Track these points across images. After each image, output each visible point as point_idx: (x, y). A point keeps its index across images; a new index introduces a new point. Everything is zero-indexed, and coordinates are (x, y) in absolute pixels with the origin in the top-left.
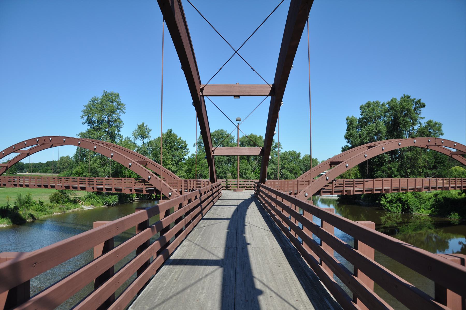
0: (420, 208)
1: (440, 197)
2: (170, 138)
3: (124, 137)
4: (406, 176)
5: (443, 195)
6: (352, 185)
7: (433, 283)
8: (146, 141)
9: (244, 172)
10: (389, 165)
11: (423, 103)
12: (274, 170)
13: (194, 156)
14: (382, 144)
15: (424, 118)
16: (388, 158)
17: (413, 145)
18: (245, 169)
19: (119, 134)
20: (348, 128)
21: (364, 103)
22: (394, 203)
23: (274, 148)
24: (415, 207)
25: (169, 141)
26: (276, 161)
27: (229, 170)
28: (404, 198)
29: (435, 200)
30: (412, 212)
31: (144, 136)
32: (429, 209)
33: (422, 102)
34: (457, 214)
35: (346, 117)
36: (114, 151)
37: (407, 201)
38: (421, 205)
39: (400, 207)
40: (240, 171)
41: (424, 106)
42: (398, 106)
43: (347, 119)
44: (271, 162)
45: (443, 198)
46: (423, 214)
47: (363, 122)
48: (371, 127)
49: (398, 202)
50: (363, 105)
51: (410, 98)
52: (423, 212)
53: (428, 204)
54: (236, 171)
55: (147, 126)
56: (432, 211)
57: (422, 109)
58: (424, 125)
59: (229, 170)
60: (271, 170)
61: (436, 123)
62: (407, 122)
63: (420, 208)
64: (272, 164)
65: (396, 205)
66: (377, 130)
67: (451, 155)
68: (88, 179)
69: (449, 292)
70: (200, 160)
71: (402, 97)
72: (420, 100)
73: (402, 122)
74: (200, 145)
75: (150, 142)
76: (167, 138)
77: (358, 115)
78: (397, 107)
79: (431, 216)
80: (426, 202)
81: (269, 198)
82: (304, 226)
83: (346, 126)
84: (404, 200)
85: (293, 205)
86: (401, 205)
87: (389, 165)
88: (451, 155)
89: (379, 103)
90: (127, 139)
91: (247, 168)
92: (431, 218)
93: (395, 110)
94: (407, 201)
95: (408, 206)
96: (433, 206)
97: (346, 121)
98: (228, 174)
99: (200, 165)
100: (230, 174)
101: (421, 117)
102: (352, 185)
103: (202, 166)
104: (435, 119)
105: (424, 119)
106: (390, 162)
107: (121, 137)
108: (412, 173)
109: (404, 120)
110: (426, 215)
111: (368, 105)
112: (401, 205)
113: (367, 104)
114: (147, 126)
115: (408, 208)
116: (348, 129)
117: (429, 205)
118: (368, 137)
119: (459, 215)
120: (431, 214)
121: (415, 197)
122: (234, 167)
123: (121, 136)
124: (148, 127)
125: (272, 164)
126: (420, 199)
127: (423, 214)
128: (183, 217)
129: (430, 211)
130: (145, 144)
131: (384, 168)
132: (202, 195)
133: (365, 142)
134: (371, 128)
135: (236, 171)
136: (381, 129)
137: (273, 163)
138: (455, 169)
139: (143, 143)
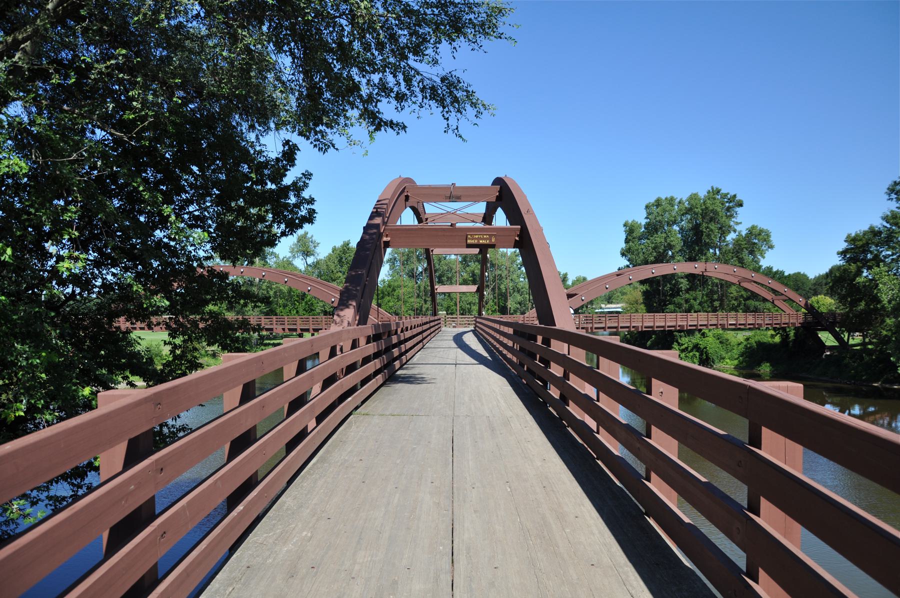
0: (724, 358)
1: (752, 341)
2: (348, 255)
3: (281, 257)
4: (715, 310)
5: (757, 338)
6: (591, 321)
7: (563, 369)
8: (310, 260)
9: (468, 309)
10: (687, 296)
11: (740, 200)
12: (520, 303)
13: (384, 283)
14: (630, 273)
15: (741, 223)
16: (684, 284)
17: (674, 272)
18: (470, 304)
19: (272, 252)
20: (626, 239)
21: (652, 200)
22: (689, 352)
23: (519, 266)
24: (717, 357)
25: (346, 259)
26: (524, 289)
27: (442, 305)
28: (702, 344)
29: (745, 346)
30: (712, 364)
31: (307, 253)
32: (736, 359)
33: (738, 198)
34: (768, 364)
35: (623, 222)
36: (311, 284)
37: (706, 348)
38: (727, 353)
39: (696, 357)
40: (461, 307)
41: (740, 205)
42: (699, 206)
43: (625, 225)
44: (514, 291)
45: (756, 342)
46: (727, 366)
47: (652, 228)
48: (658, 239)
49: (695, 350)
50: (650, 203)
51: (721, 192)
52: (727, 363)
53: (736, 352)
54: (454, 307)
55: (312, 236)
56: (739, 361)
57: (738, 209)
58: (744, 233)
59: (442, 305)
60: (515, 305)
61: (761, 231)
62: (712, 230)
63: (724, 358)
64: (516, 294)
65: (691, 354)
66: (666, 242)
67: (740, 283)
68: (313, 318)
69: (571, 374)
70: (394, 290)
71: (709, 191)
72: (735, 196)
73: (704, 230)
74: (394, 264)
75: (318, 262)
76: (343, 255)
77: (641, 218)
78: (697, 208)
79: (737, 368)
80: (734, 349)
81: (508, 351)
82: (600, 427)
83: (624, 236)
84: (701, 346)
85: (498, 335)
86: (697, 354)
87: (687, 296)
88: (740, 283)
89: (675, 200)
90: (285, 259)
91: (474, 302)
92: (737, 371)
93: (695, 212)
94: (706, 348)
95: (707, 356)
96: (742, 355)
97: (624, 229)
98: (440, 312)
99: (395, 297)
100: (445, 312)
101: (736, 221)
102: (591, 321)
103: (398, 298)
104: (762, 225)
105: (740, 225)
106: (687, 291)
107: (276, 256)
108: (722, 307)
109: (708, 227)
110: (730, 368)
111: (658, 203)
112: (697, 354)
113: (656, 201)
114: (312, 236)
115: (708, 358)
116: (627, 241)
117: (736, 354)
118: (655, 254)
119: (771, 365)
120: (737, 365)
121: (720, 342)
122: (452, 300)
123: (276, 254)
124: (313, 238)
125: (516, 294)
126: (727, 345)
127: (727, 366)
128: (359, 387)
129: (736, 362)
130: (310, 266)
131: (677, 300)
132: (358, 367)
133: (649, 260)
134: (659, 240)
135: (454, 307)
136: (672, 241)
137: (519, 291)
138: (817, 300)
139: (306, 265)
